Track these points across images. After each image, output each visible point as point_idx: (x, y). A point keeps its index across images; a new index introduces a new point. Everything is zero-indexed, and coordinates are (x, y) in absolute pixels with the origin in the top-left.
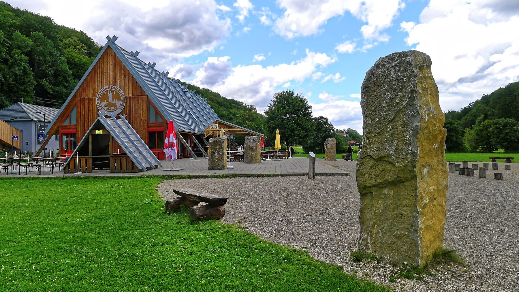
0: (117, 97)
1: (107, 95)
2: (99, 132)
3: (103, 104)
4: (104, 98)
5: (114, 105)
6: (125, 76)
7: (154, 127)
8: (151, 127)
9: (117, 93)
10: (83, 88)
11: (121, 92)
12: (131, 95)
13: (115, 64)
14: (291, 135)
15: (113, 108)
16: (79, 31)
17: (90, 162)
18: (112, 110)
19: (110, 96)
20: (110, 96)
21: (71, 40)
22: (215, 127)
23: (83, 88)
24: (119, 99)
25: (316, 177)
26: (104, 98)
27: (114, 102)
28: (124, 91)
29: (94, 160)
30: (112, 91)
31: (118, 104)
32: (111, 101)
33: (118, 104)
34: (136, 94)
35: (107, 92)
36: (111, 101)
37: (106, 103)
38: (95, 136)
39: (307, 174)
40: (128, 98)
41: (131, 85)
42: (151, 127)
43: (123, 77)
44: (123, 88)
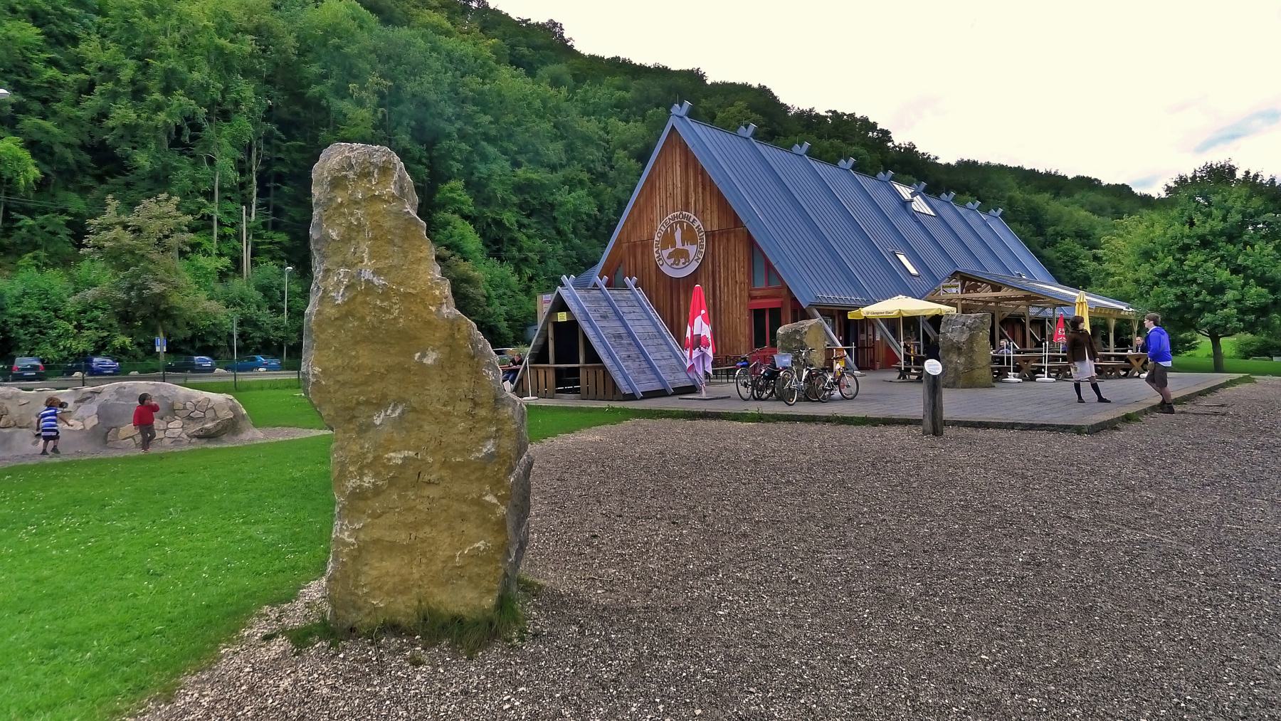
0: (689, 236)
1: (673, 232)
2: (562, 317)
3: (665, 253)
4: (668, 240)
5: (684, 254)
6: (704, 188)
7: (762, 297)
8: (755, 298)
9: (690, 228)
10: (634, 222)
11: (698, 223)
12: (715, 228)
13: (687, 165)
14: (1211, 303)
15: (682, 260)
16: (755, 85)
17: (551, 376)
18: (681, 265)
19: (678, 235)
20: (678, 235)
21: (732, 109)
22: (954, 290)
23: (634, 222)
24: (694, 242)
25: (949, 431)
26: (668, 240)
27: (686, 247)
28: (703, 222)
29: (557, 371)
30: (681, 223)
31: (692, 249)
32: (679, 245)
33: (692, 249)
34: (724, 227)
35: (671, 226)
36: (679, 245)
37: (671, 250)
38: (557, 325)
39: (918, 422)
40: (710, 235)
41: (715, 206)
42: (755, 298)
43: (700, 190)
44: (700, 214)
